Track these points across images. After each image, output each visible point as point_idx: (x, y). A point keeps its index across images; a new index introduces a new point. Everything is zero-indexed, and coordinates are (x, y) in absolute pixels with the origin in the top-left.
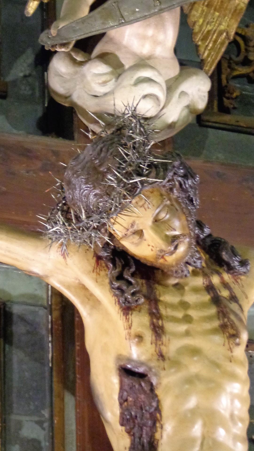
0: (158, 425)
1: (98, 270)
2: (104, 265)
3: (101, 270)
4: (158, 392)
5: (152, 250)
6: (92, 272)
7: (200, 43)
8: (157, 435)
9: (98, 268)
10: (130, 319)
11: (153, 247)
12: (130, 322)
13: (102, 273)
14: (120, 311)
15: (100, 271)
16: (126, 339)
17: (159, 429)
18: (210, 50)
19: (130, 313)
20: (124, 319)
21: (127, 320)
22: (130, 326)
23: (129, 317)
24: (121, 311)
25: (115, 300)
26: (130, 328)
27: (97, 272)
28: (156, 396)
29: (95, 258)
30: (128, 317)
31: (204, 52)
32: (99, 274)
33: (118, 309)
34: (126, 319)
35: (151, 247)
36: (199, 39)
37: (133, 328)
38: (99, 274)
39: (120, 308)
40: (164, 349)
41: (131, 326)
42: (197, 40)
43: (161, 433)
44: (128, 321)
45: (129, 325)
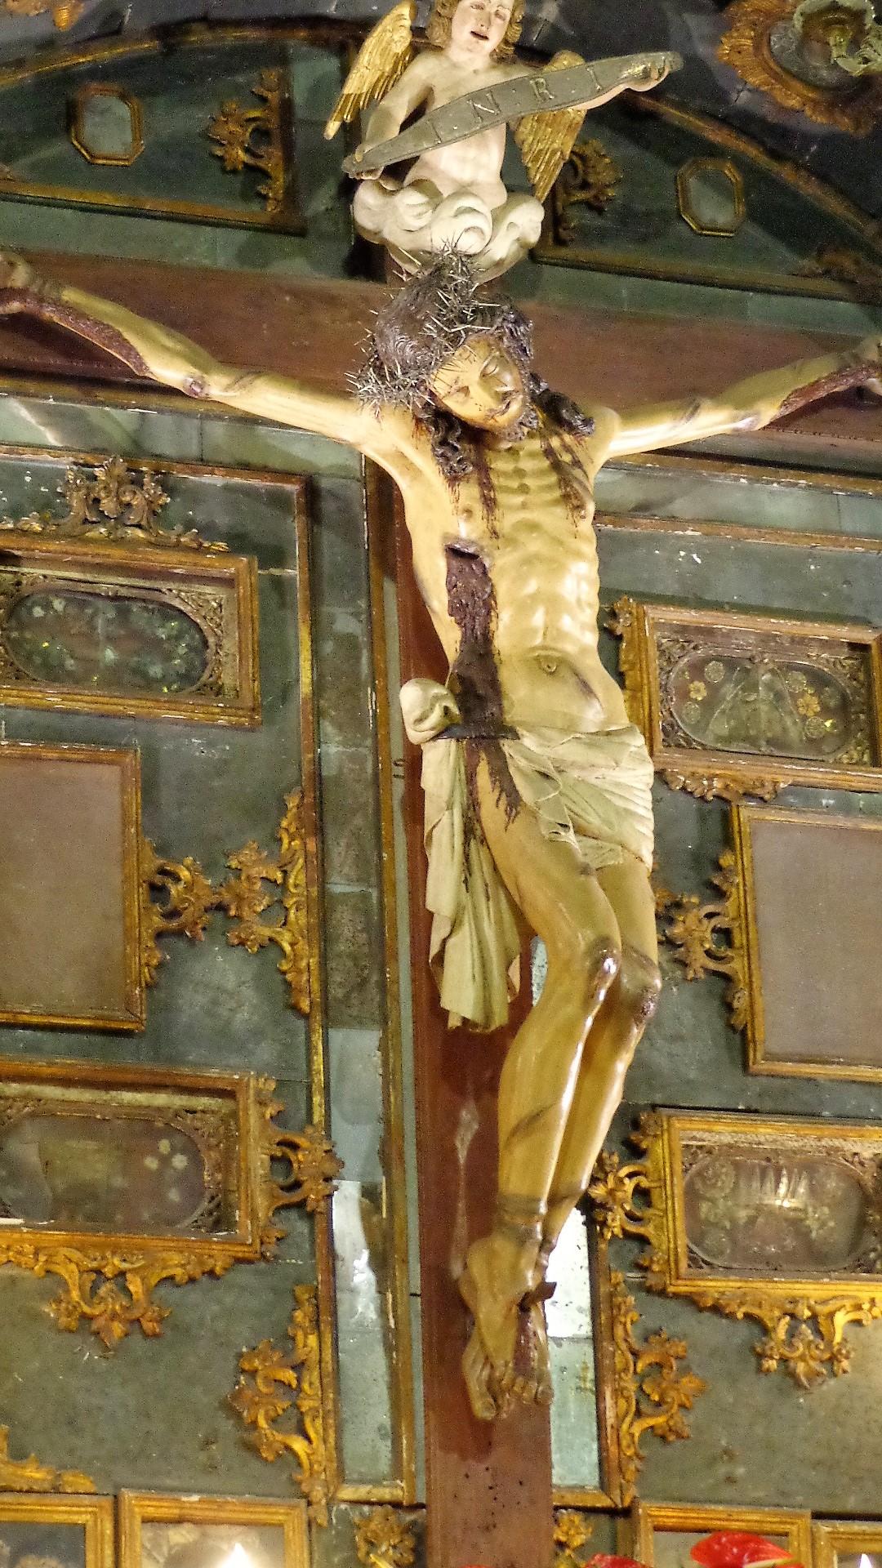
8: (492, 626)
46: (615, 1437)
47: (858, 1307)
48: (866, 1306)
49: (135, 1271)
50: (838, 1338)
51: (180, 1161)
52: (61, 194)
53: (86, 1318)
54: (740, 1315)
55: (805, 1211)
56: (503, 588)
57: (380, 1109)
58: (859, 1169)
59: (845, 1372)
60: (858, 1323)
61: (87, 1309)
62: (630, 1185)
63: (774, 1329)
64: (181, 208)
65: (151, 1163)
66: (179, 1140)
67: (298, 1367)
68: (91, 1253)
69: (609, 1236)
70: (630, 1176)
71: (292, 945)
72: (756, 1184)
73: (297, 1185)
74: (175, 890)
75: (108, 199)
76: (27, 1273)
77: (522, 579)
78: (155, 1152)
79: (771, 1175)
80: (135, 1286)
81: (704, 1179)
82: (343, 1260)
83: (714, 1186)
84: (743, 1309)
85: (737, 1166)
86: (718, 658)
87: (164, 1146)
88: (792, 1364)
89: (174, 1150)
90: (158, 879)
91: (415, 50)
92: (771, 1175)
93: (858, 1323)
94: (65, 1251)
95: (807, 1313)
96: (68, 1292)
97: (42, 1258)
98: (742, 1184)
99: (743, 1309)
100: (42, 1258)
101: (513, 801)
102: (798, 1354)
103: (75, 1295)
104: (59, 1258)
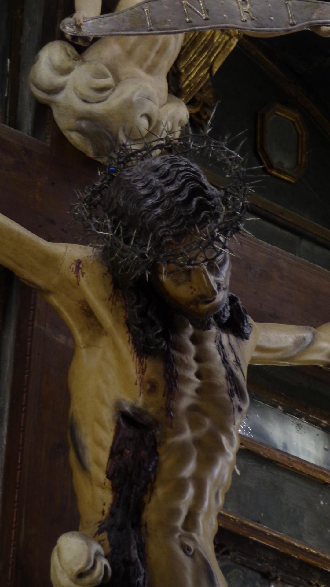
0: (149, 486)
1: (115, 300)
2: (121, 295)
3: (118, 301)
4: (160, 450)
5: (192, 293)
6: (107, 300)
7: (183, 71)
8: (146, 498)
9: (115, 297)
10: (144, 364)
11: (195, 290)
12: (144, 366)
13: (119, 304)
14: (133, 351)
15: (117, 302)
16: (136, 384)
17: (149, 492)
18: (190, 81)
19: (145, 356)
20: (138, 362)
21: (141, 363)
22: (144, 370)
23: (143, 361)
24: (135, 351)
25: (129, 337)
26: (143, 373)
27: (113, 302)
28: (157, 454)
29: (112, 286)
30: (142, 360)
31: (185, 82)
32: (115, 305)
33: (132, 349)
34: (140, 361)
35: (192, 290)
36: (184, 67)
37: (146, 373)
38: (115, 305)
39: (134, 348)
41: (145, 371)
42: (181, 67)
43: (150, 497)
44: (142, 365)
45: (142, 369)
82: (146, 525)
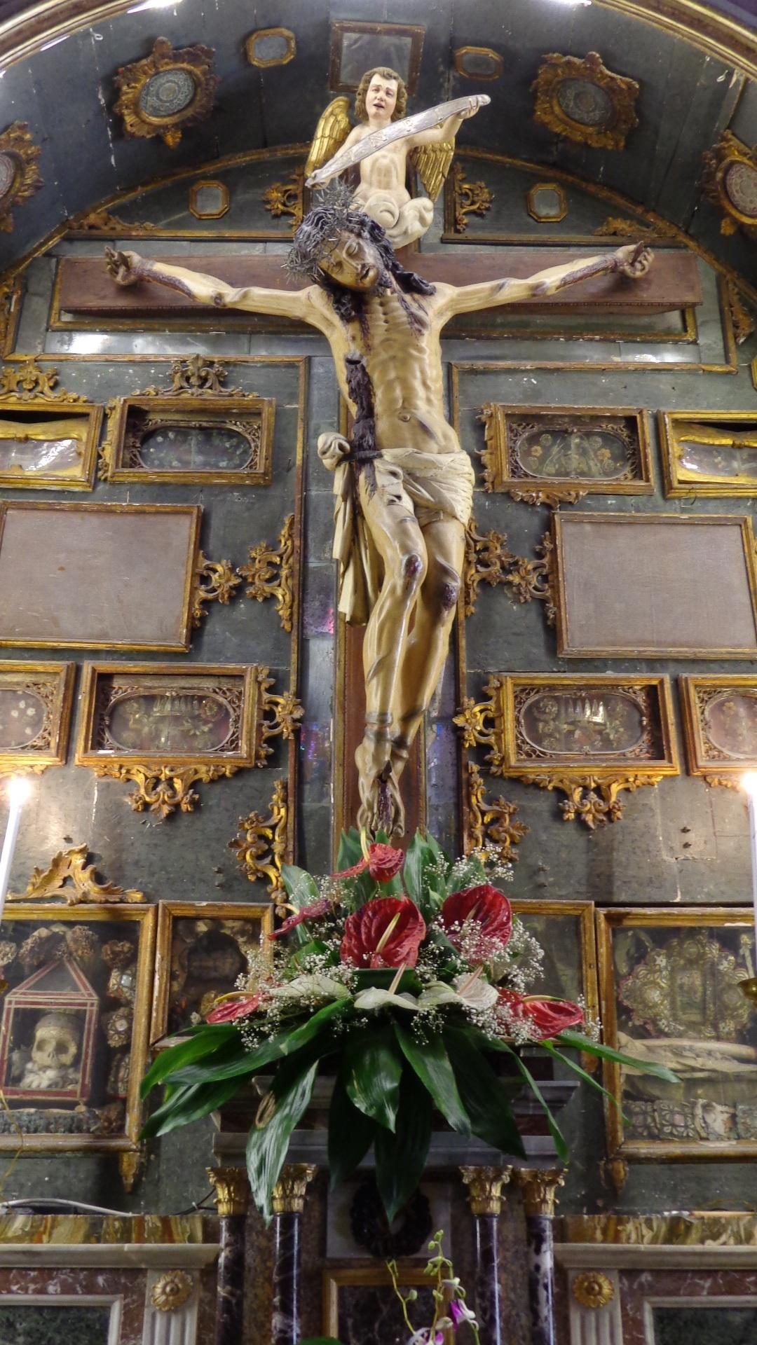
8: (373, 400)
40: (370, 342)
46: (50, 917)
47: (627, 781)
48: (631, 779)
49: (178, 777)
50: (613, 799)
51: (31, 712)
52: (180, 233)
53: (146, 806)
54: (550, 788)
55: (604, 725)
56: (375, 377)
57: (332, 683)
58: (633, 696)
59: (618, 819)
60: (627, 790)
61: (148, 799)
62: (480, 718)
63: (572, 795)
64: (245, 234)
65: (15, 714)
66: (31, 701)
67: (273, 828)
68: (153, 767)
69: (467, 745)
70: (481, 711)
71: (283, 596)
72: (571, 710)
73: (277, 725)
74: (215, 577)
75: (205, 234)
76: (116, 780)
77: (384, 371)
78: (17, 708)
79: (579, 703)
80: (178, 784)
81: (538, 708)
83: (544, 712)
84: (552, 785)
85: (557, 699)
86: (547, 432)
87: (22, 705)
88: (584, 815)
89: (27, 706)
90: (205, 573)
91: (352, 125)
92: (579, 703)
93: (627, 790)
94: (137, 767)
95: (593, 785)
96: (138, 790)
97: (124, 771)
98: (563, 711)
99: (552, 785)
100: (124, 771)
101: (373, 486)
102: (587, 809)
103: (142, 791)
104: (134, 771)
